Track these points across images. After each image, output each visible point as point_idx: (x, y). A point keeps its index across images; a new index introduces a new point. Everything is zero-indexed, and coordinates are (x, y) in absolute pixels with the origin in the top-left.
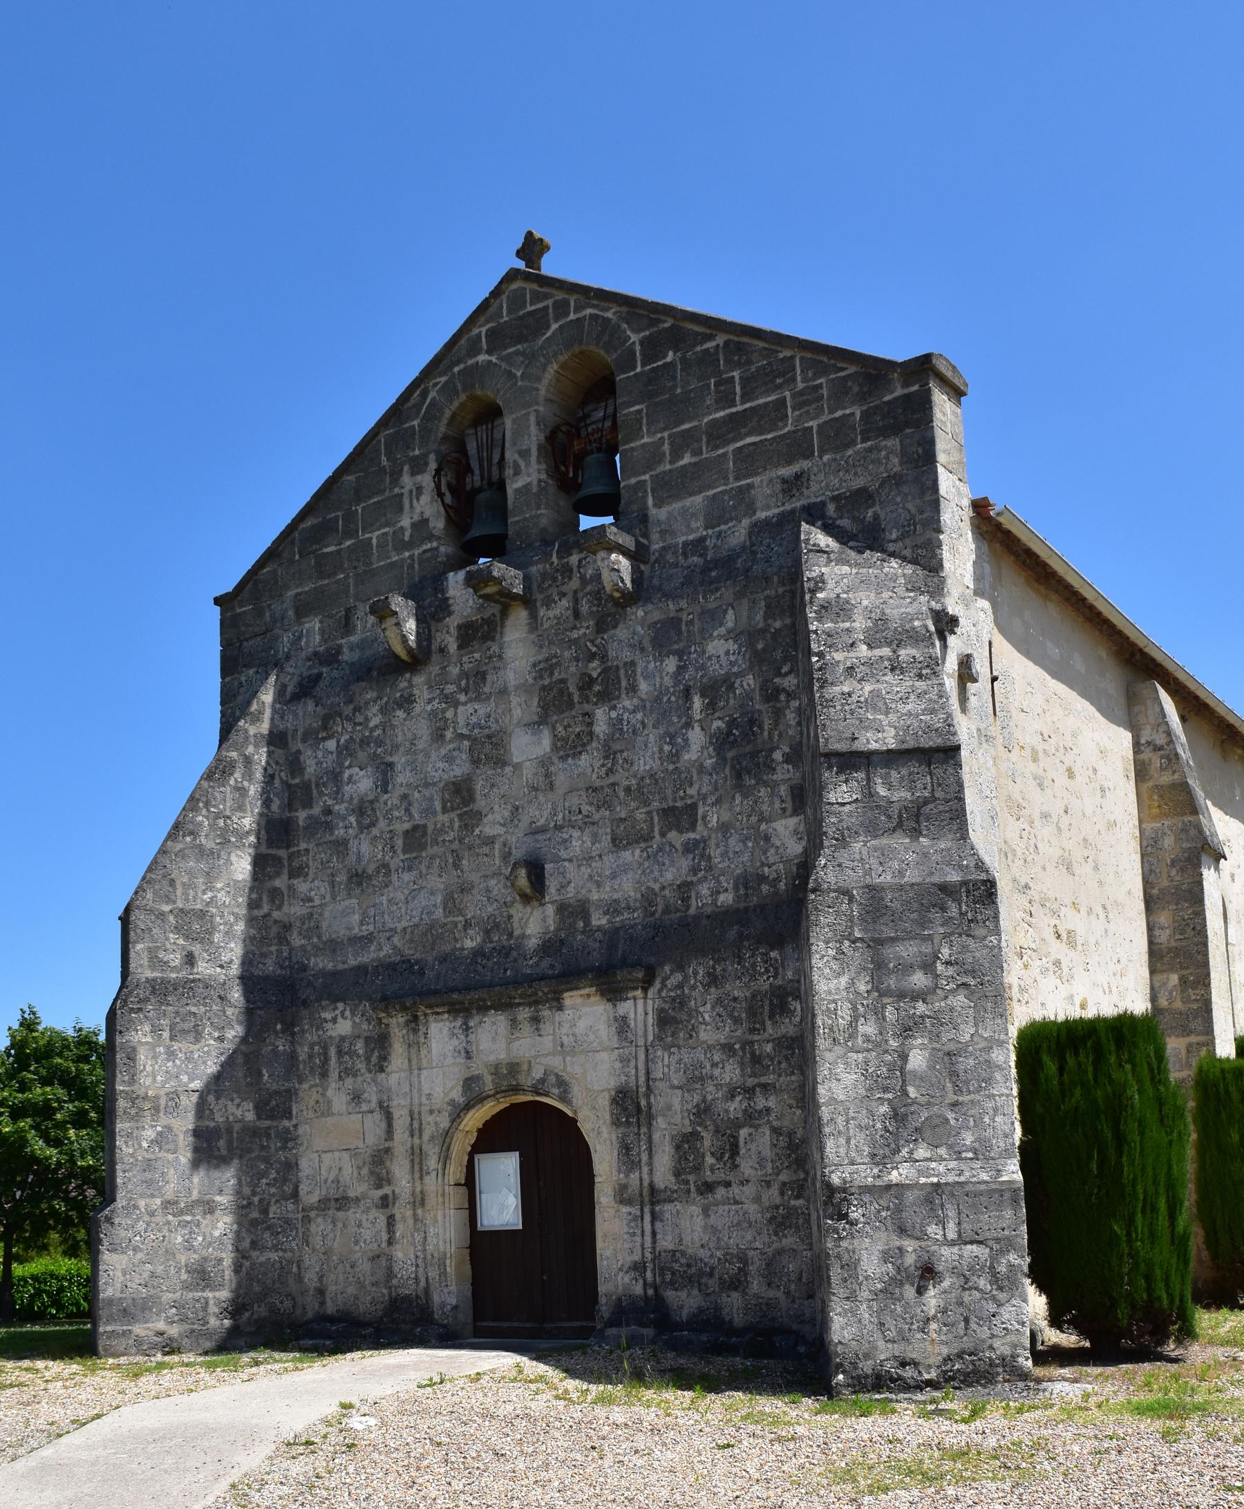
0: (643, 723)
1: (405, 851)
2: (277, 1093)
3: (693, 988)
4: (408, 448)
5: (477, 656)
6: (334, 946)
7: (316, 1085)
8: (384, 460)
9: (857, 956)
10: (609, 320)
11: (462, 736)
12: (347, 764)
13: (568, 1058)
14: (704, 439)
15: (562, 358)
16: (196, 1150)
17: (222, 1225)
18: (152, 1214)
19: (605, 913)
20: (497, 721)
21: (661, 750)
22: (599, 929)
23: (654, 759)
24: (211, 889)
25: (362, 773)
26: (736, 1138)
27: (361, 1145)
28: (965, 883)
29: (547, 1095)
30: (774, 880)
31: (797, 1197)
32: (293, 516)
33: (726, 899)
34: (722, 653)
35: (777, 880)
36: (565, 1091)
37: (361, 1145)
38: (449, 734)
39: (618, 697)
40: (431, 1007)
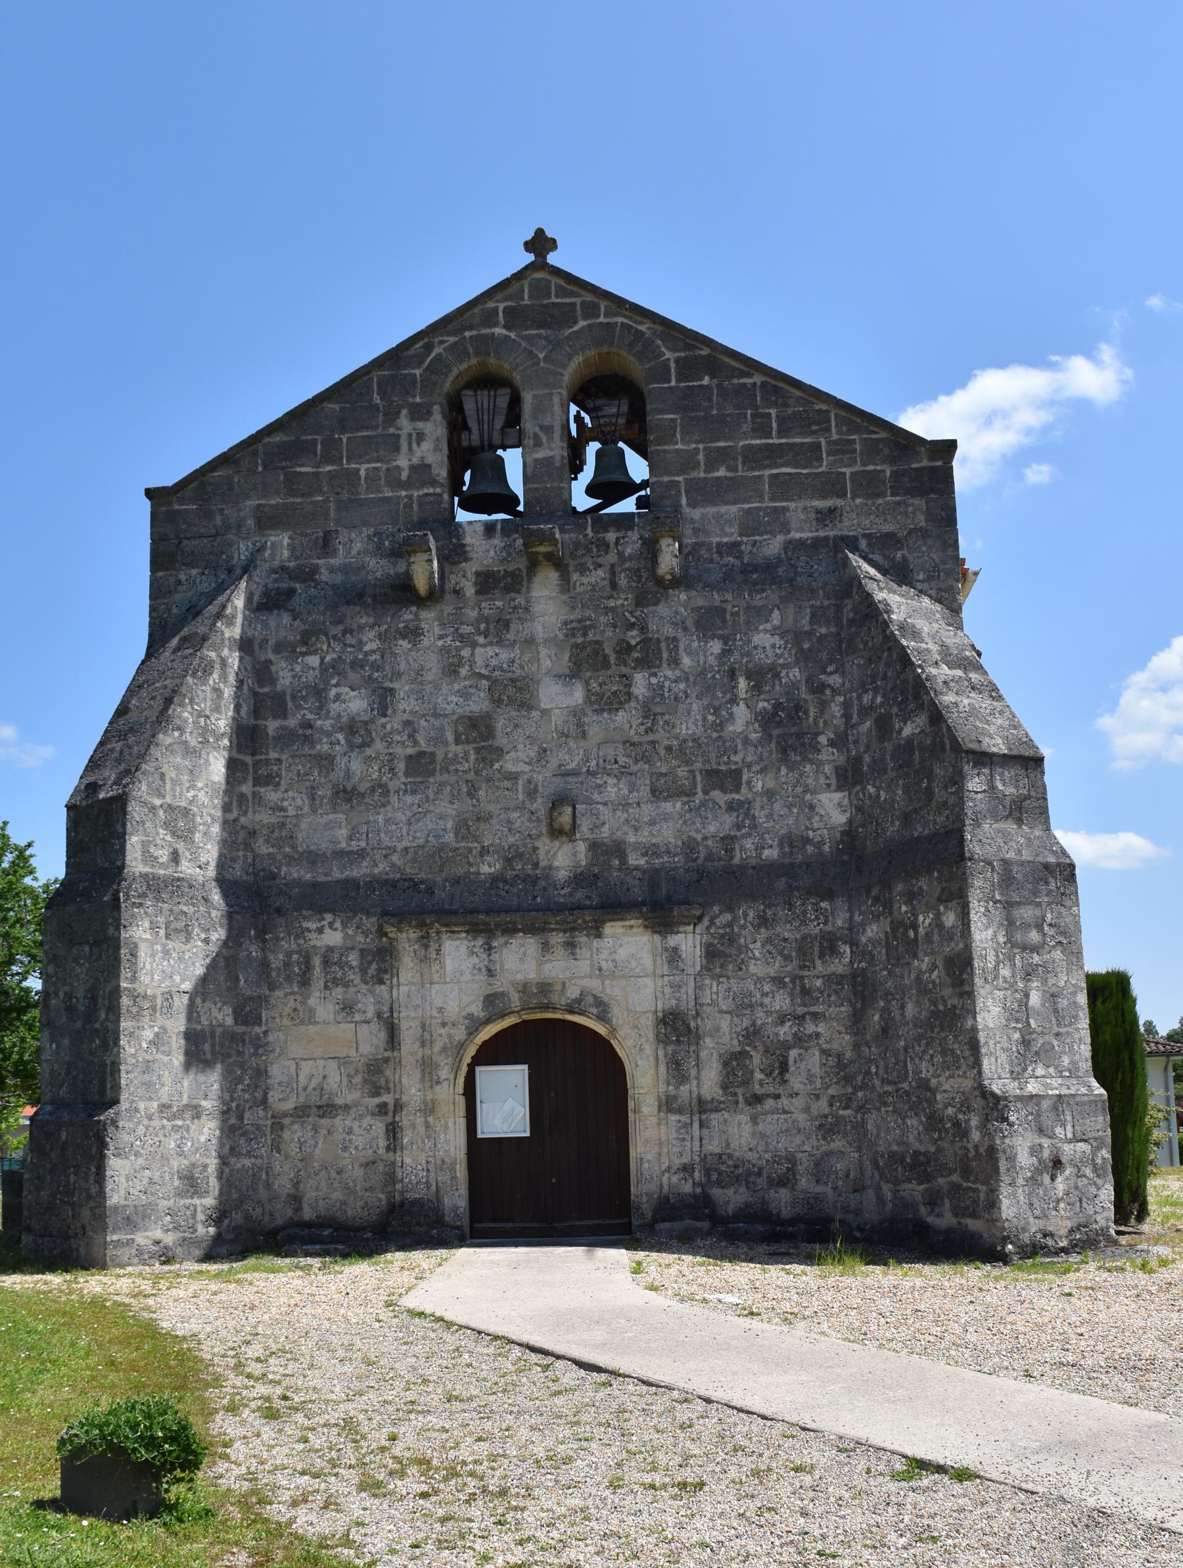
0: (685, 692)
1: (407, 775)
2: (251, 998)
3: (744, 927)
4: (407, 393)
5: (499, 604)
6: (313, 858)
7: (294, 993)
8: (377, 399)
9: (998, 914)
10: (643, 333)
11: (480, 676)
12: (334, 682)
13: (607, 982)
14: (740, 460)
15: (589, 353)
16: (187, 1053)
17: (207, 1130)
18: (150, 1118)
19: (643, 855)
20: (522, 668)
21: (704, 719)
22: (637, 868)
23: (697, 726)
24: (193, 787)
25: (353, 694)
26: (786, 1058)
27: (353, 1053)
28: (1059, 864)
29: (582, 1013)
30: (819, 843)
31: (845, 1108)
32: (260, 427)
33: (771, 854)
34: (767, 645)
35: (822, 843)
36: (605, 1011)
37: (353, 1053)
38: (464, 671)
39: (659, 666)
40: (447, 925)
